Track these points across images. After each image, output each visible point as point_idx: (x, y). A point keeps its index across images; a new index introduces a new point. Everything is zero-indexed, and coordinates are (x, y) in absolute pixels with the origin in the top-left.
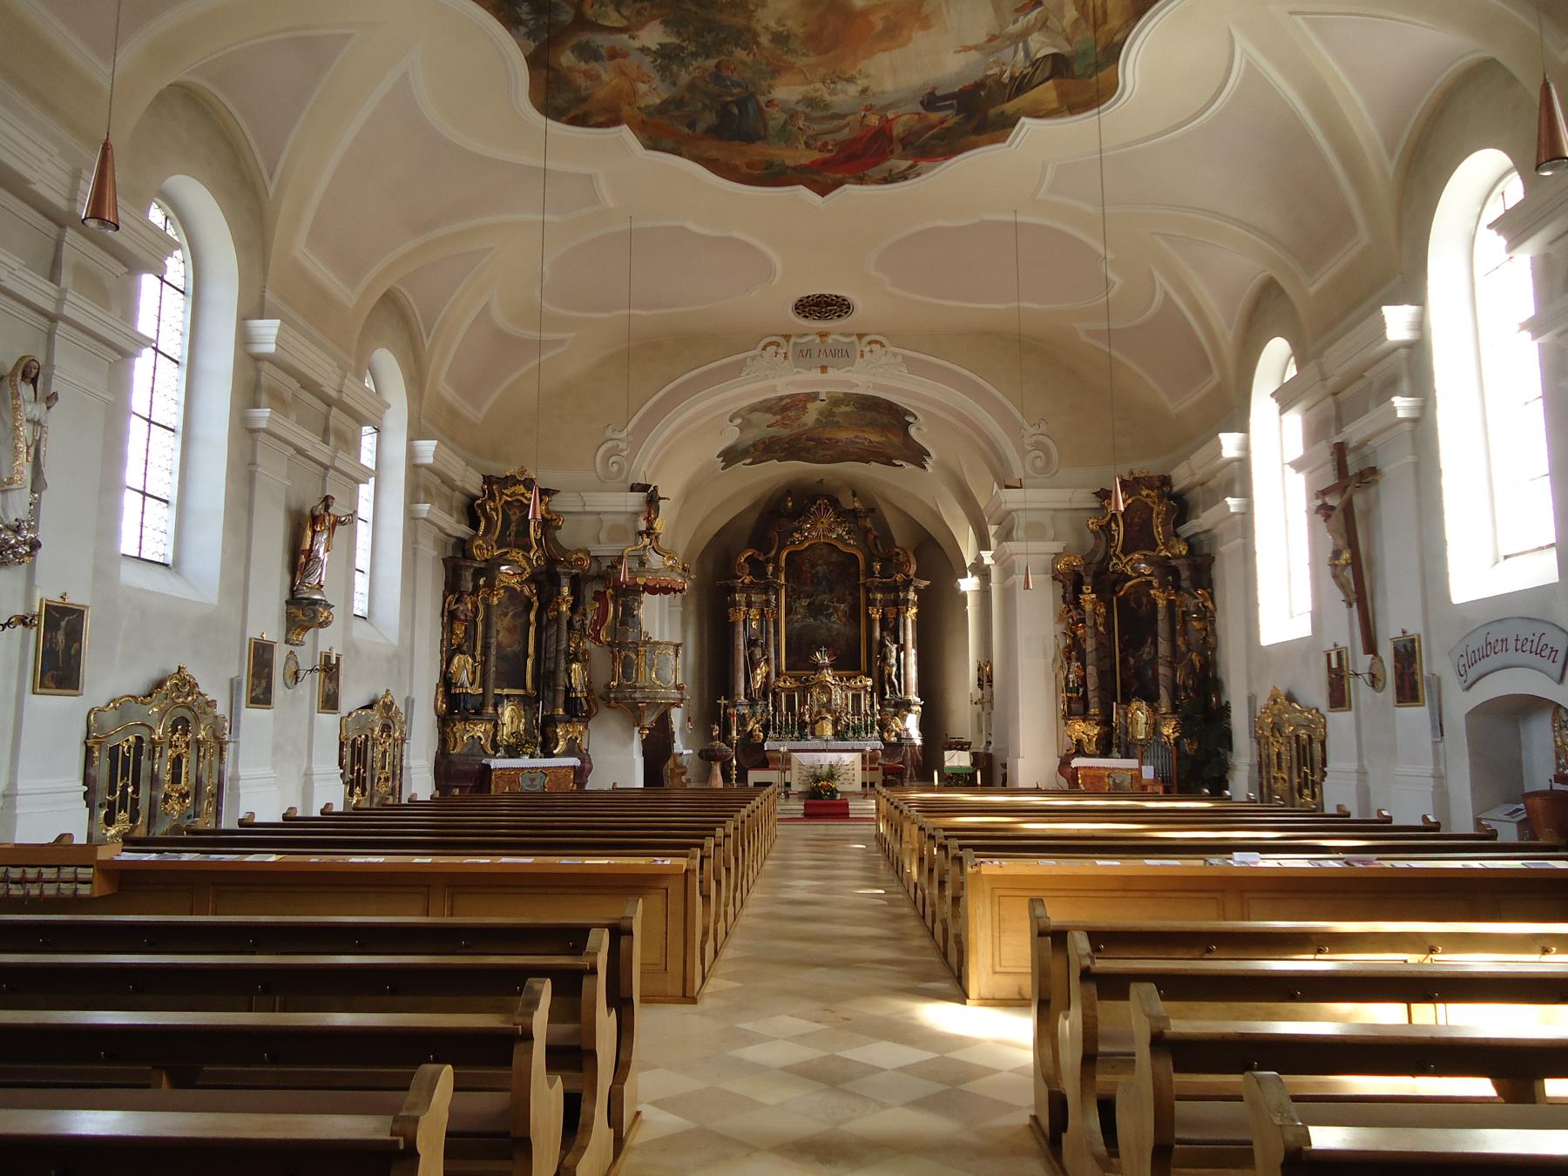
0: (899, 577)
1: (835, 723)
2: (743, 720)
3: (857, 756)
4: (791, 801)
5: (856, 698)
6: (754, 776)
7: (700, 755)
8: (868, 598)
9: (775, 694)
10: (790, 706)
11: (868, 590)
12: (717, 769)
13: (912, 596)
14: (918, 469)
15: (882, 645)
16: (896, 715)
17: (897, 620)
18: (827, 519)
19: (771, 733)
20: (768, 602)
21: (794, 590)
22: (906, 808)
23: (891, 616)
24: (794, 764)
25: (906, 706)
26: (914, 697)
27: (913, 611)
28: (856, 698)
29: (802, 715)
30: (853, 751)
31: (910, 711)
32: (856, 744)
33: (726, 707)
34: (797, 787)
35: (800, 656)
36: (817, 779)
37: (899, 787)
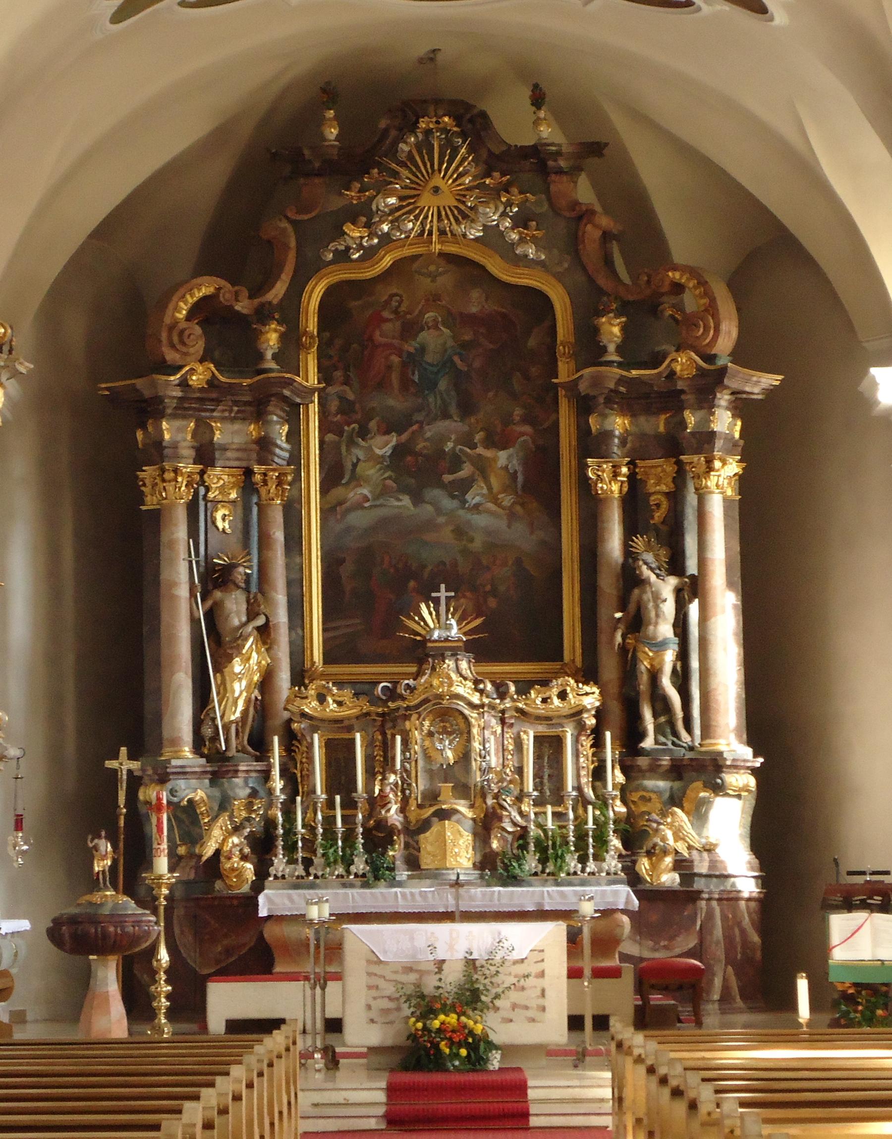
0: (683, 363)
1: (485, 826)
2: (188, 820)
3: (553, 934)
4: (343, 1077)
5: (550, 747)
6: (227, 1000)
7: (54, 934)
8: (584, 432)
9: (291, 739)
10: (340, 776)
11: (585, 406)
12: (108, 977)
13: (725, 422)
14: (742, 17)
15: (630, 579)
16: (675, 800)
17: (676, 498)
18: (451, 179)
19: (279, 863)
20: (264, 445)
21: (346, 408)
22: (706, 1094)
23: (658, 487)
24: (353, 962)
25: (708, 770)
26: (731, 743)
27: (726, 473)
28: (550, 747)
29: (377, 803)
30: (541, 915)
31: (719, 789)
32: (550, 895)
33: (135, 782)
34: (361, 1034)
35: (370, 610)
36: (428, 1006)
37: (688, 1029)
